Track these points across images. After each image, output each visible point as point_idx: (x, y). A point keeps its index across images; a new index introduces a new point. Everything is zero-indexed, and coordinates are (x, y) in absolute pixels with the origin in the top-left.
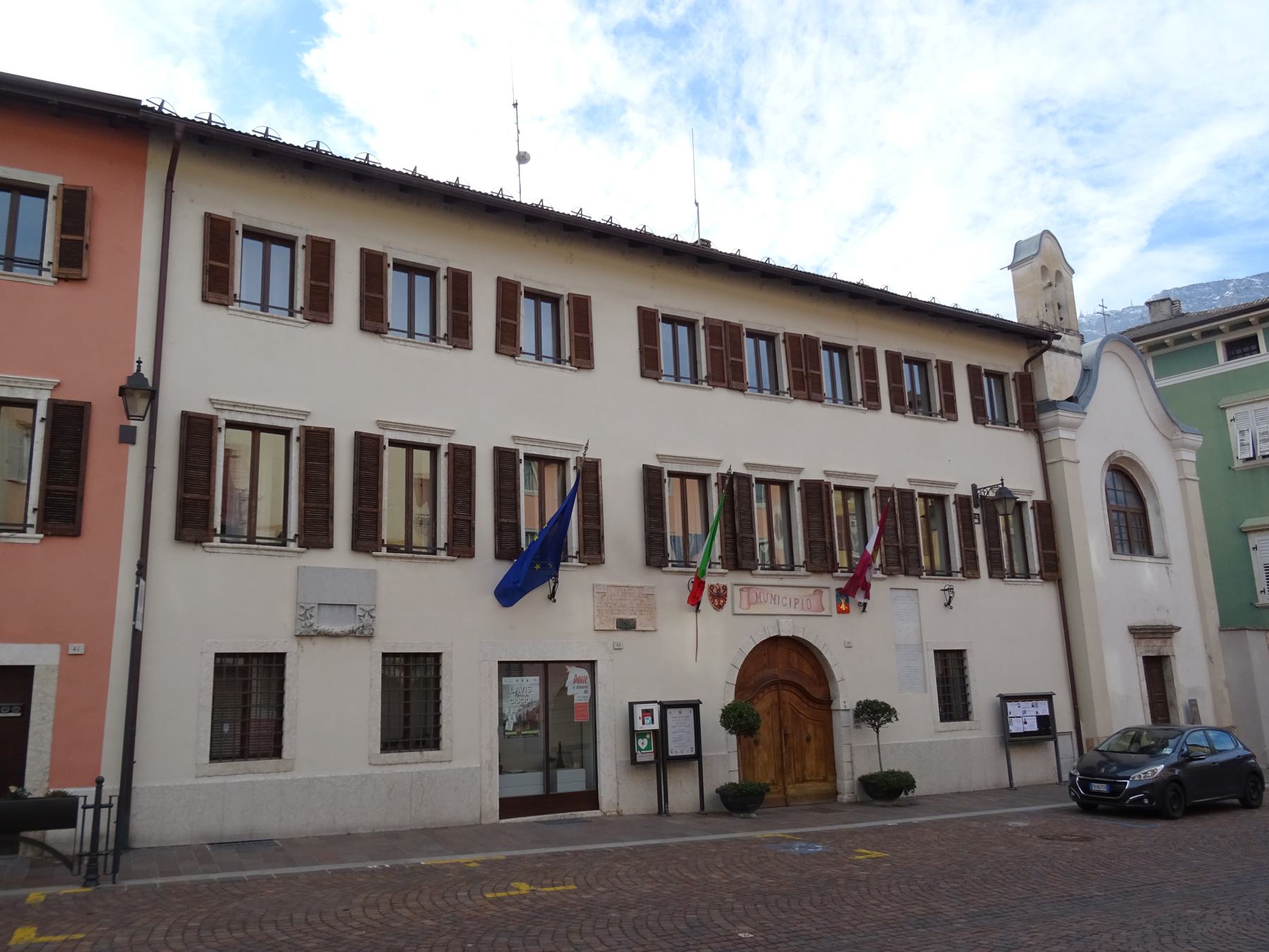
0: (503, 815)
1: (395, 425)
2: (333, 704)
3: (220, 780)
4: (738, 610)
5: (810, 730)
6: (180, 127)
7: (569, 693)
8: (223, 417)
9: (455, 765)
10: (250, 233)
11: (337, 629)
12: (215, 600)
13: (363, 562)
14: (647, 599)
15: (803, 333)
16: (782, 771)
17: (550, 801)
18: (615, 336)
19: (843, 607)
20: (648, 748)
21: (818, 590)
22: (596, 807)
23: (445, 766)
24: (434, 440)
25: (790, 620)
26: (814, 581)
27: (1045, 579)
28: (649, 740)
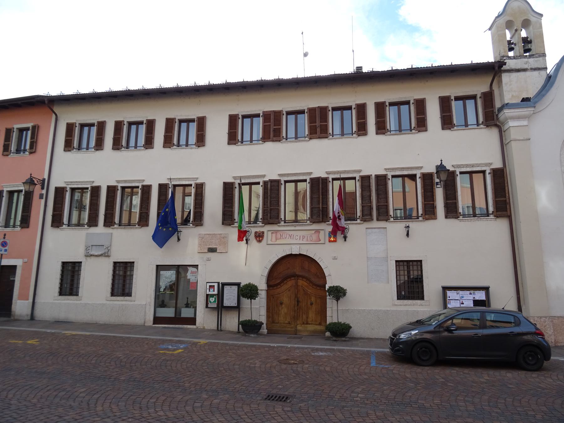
0: (155, 323)
1: (122, 181)
2: (96, 279)
3: (59, 301)
4: (270, 242)
5: (313, 299)
6: (46, 100)
7: (188, 278)
8: (331, 177)
9: (136, 303)
10: (457, 99)
11: (96, 254)
12: (64, 243)
13: (108, 230)
14: (224, 240)
15: (317, 106)
16: (295, 318)
17: (177, 320)
18: (217, 129)
19: (332, 239)
20: (215, 302)
21: (318, 231)
22: (195, 324)
23: (132, 303)
24: (483, 169)
25: (298, 246)
26: (315, 227)
27: (497, 217)
28: (215, 299)
